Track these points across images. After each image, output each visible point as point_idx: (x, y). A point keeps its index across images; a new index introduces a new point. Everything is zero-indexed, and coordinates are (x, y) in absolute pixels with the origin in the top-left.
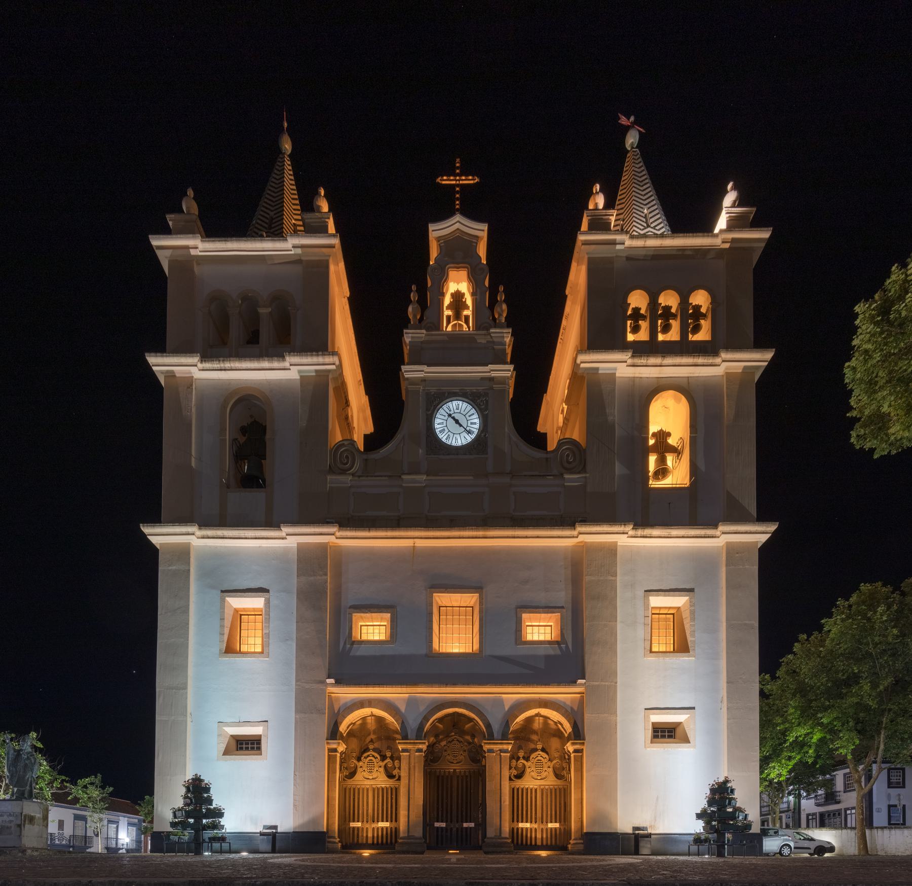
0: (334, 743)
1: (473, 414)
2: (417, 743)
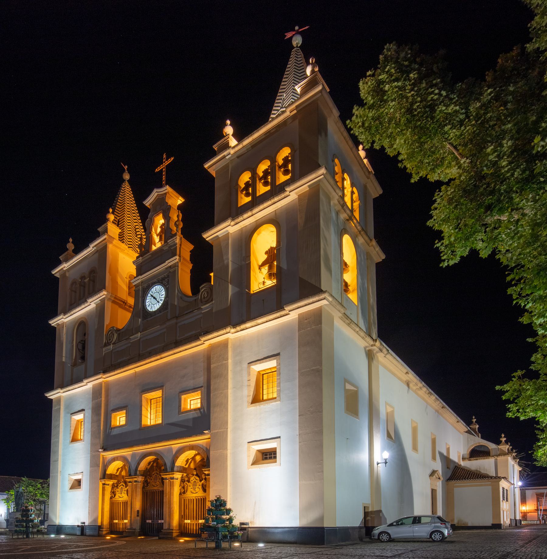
0: (103, 481)
2: (133, 478)
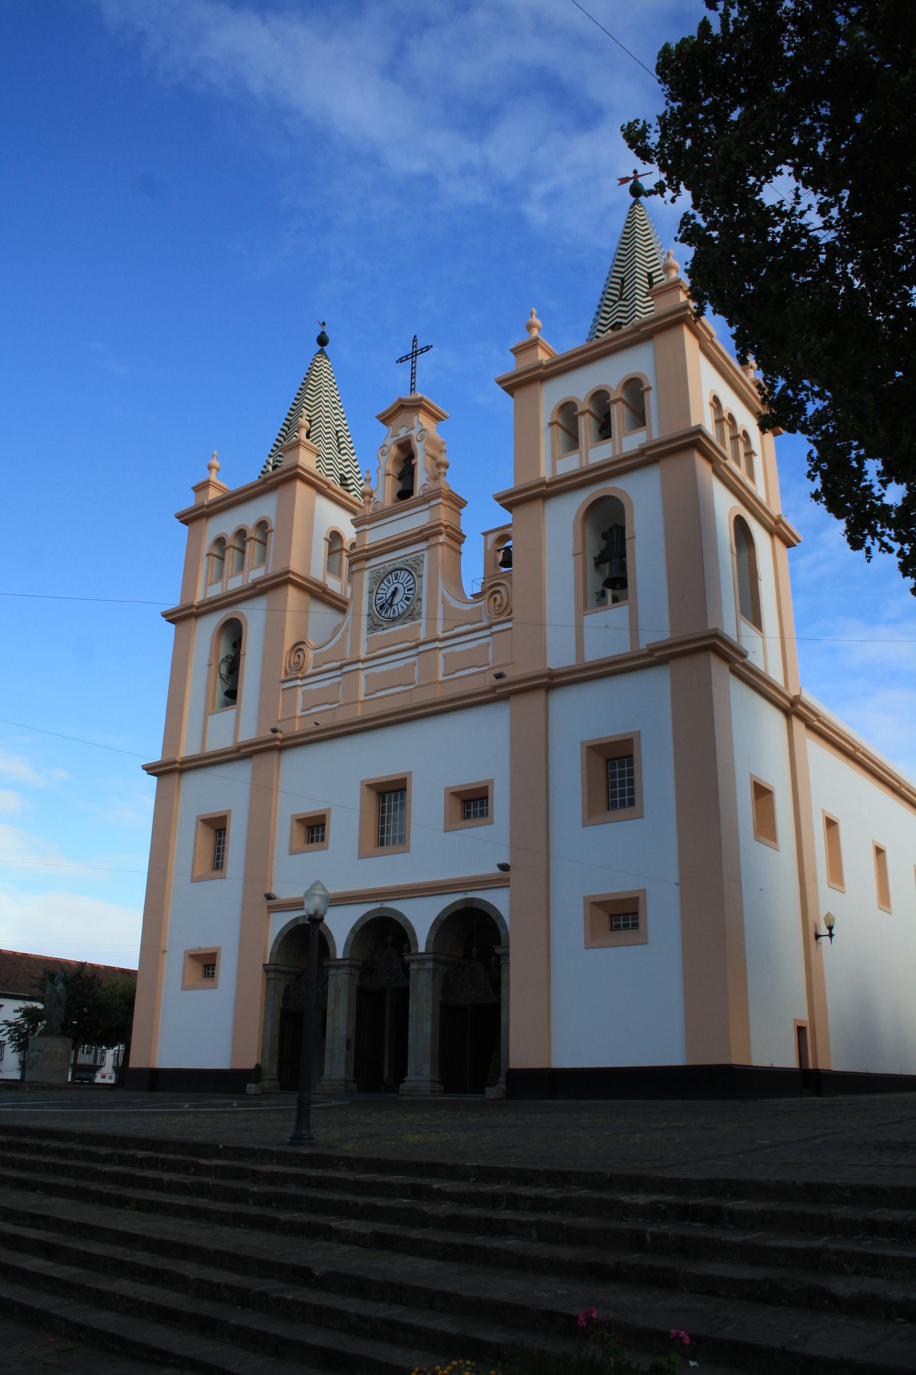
1: (410, 580)
